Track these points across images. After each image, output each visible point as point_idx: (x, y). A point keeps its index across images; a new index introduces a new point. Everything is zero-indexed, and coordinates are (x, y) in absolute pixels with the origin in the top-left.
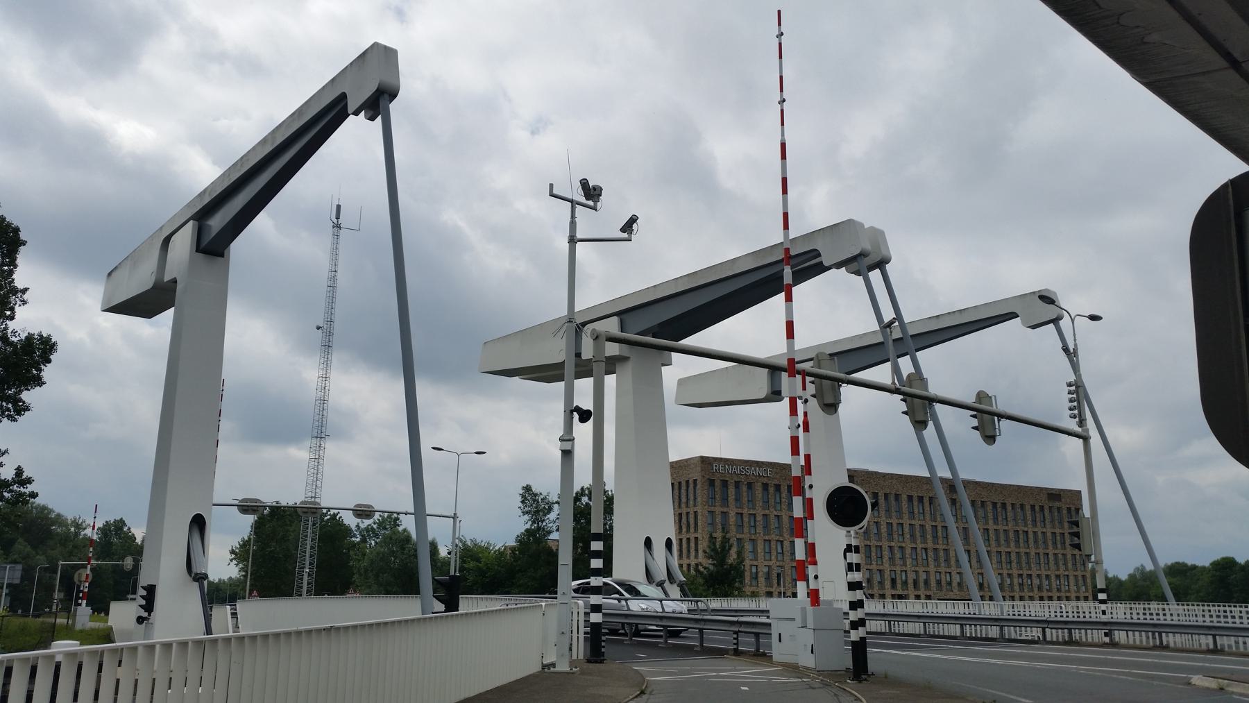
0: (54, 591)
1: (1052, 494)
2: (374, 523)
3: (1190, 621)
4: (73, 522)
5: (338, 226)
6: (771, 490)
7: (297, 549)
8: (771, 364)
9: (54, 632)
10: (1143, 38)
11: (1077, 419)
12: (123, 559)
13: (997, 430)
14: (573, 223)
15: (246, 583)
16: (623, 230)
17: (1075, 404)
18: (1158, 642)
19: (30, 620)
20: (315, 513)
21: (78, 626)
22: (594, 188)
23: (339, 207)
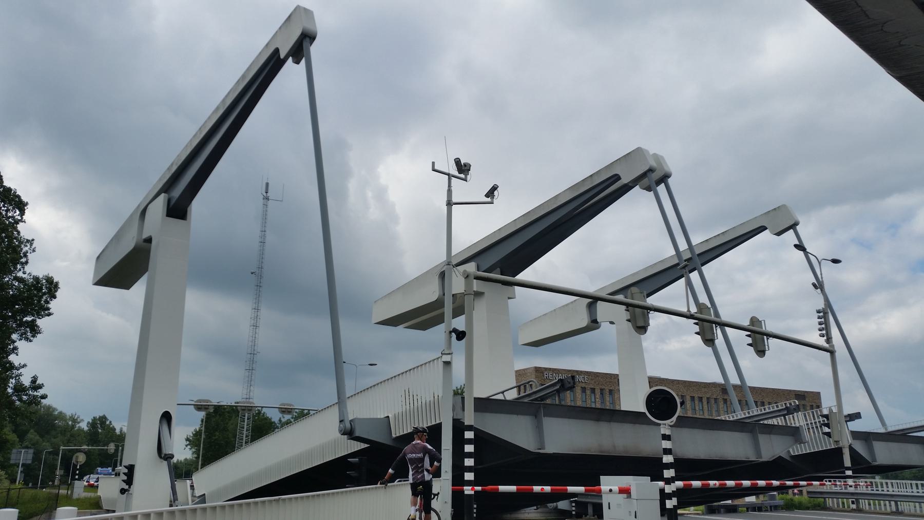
0: (56, 469)
1: (798, 394)
2: (292, 418)
3: (901, 492)
4: (70, 417)
5: (267, 198)
6: (588, 392)
7: (235, 436)
8: (597, 296)
9: (57, 500)
10: (901, 41)
11: (825, 338)
12: (107, 444)
13: (766, 346)
14: (449, 191)
15: (198, 463)
16: (487, 196)
17: (823, 326)
18: (894, 509)
19: (38, 491)
20: (250, 410)
21: (75, 496)
22: (465, 165)
23: (267, 184)
